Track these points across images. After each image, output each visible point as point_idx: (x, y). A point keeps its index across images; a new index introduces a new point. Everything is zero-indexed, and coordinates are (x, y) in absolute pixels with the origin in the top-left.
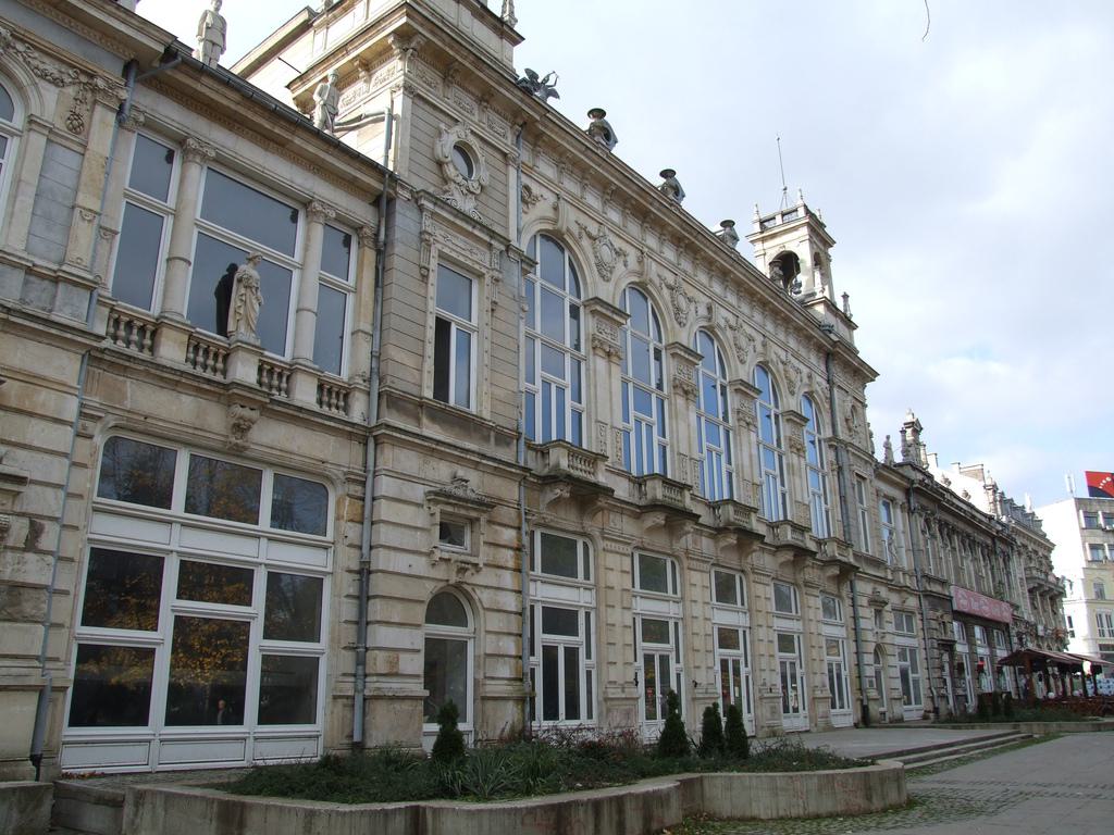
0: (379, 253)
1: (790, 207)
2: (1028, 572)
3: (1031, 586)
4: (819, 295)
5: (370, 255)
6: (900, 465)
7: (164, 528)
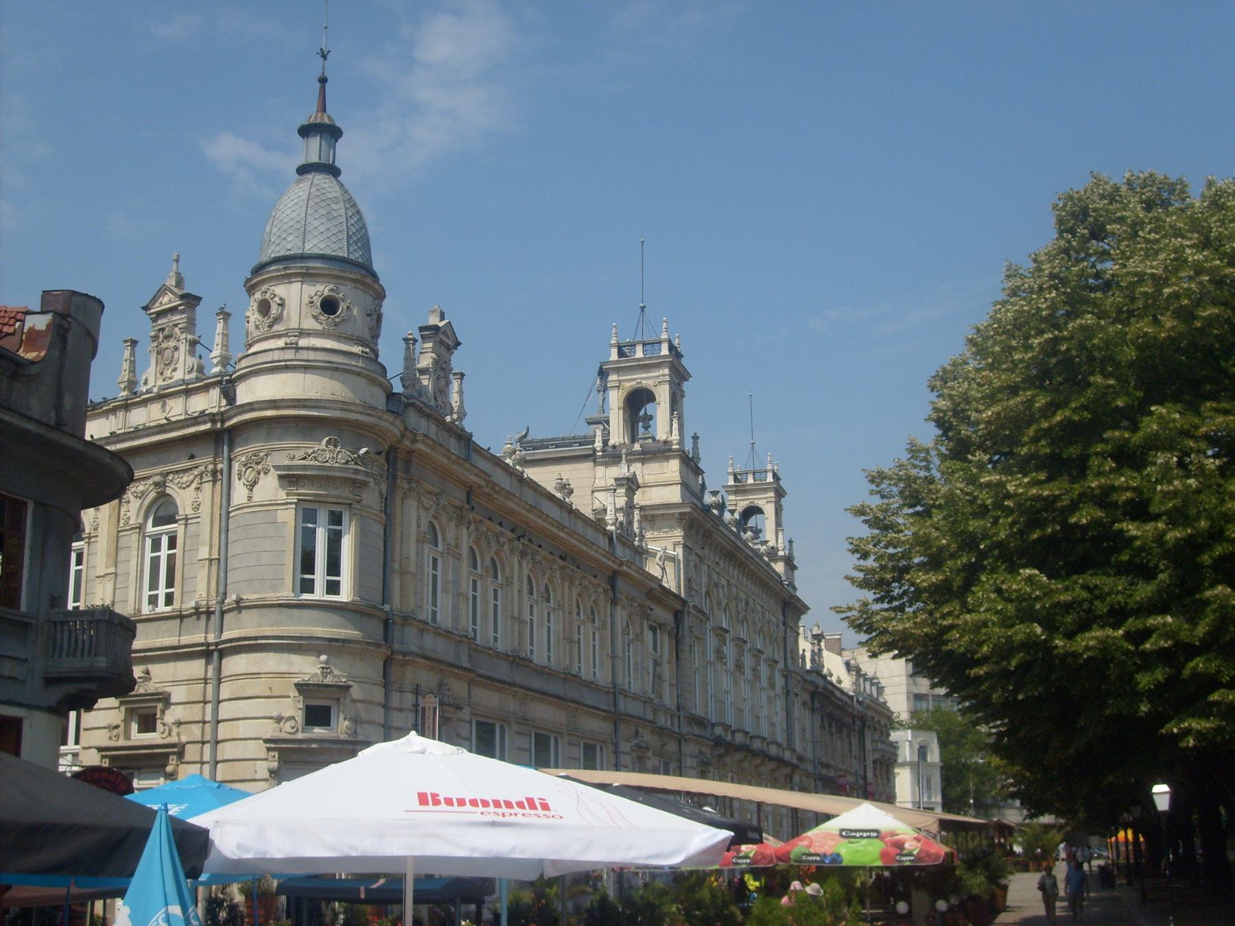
0: (677, 641)
1: (654, 338)
2: (874, 744)
3: (876, 757)
4: (781, 553)
5: (674, 641)
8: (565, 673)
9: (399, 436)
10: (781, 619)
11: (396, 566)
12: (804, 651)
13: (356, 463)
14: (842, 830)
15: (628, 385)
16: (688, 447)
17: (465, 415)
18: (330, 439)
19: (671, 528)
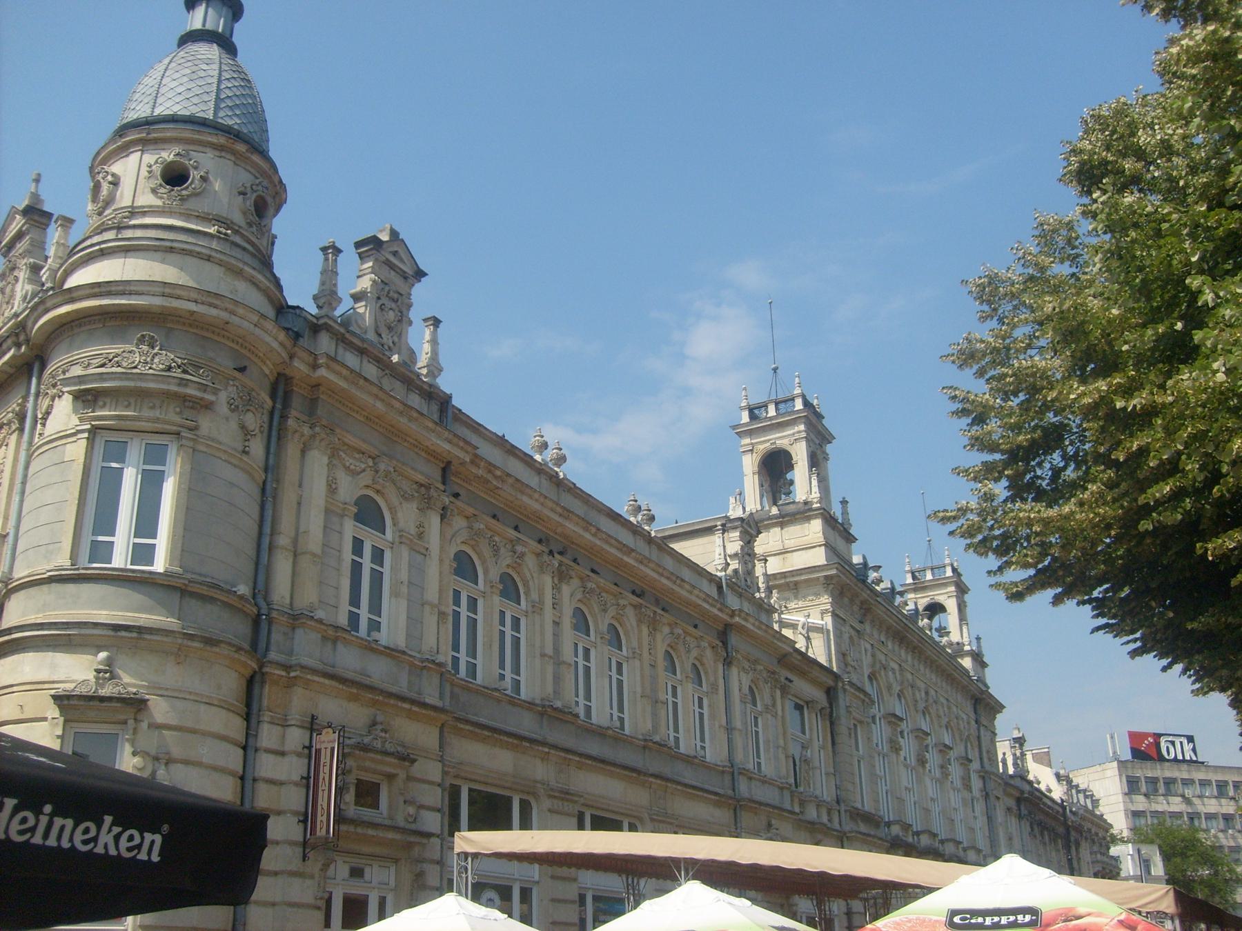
0: (832, 723)
1: (788, 395)
3: (1097, 869)
4: (967, 648)
5: (828, 723)
6: (1011, 776)
8: (645, 740)
9: (284, 355)
10: (972, 715)
11: (283, 540)
12: (1004, 754)
13: (185, 372)
14: (954, 913)
15: (761, 447)
16: (836, 510)
17: (441, 370)
18: (143, 336)
19: (817, 595)
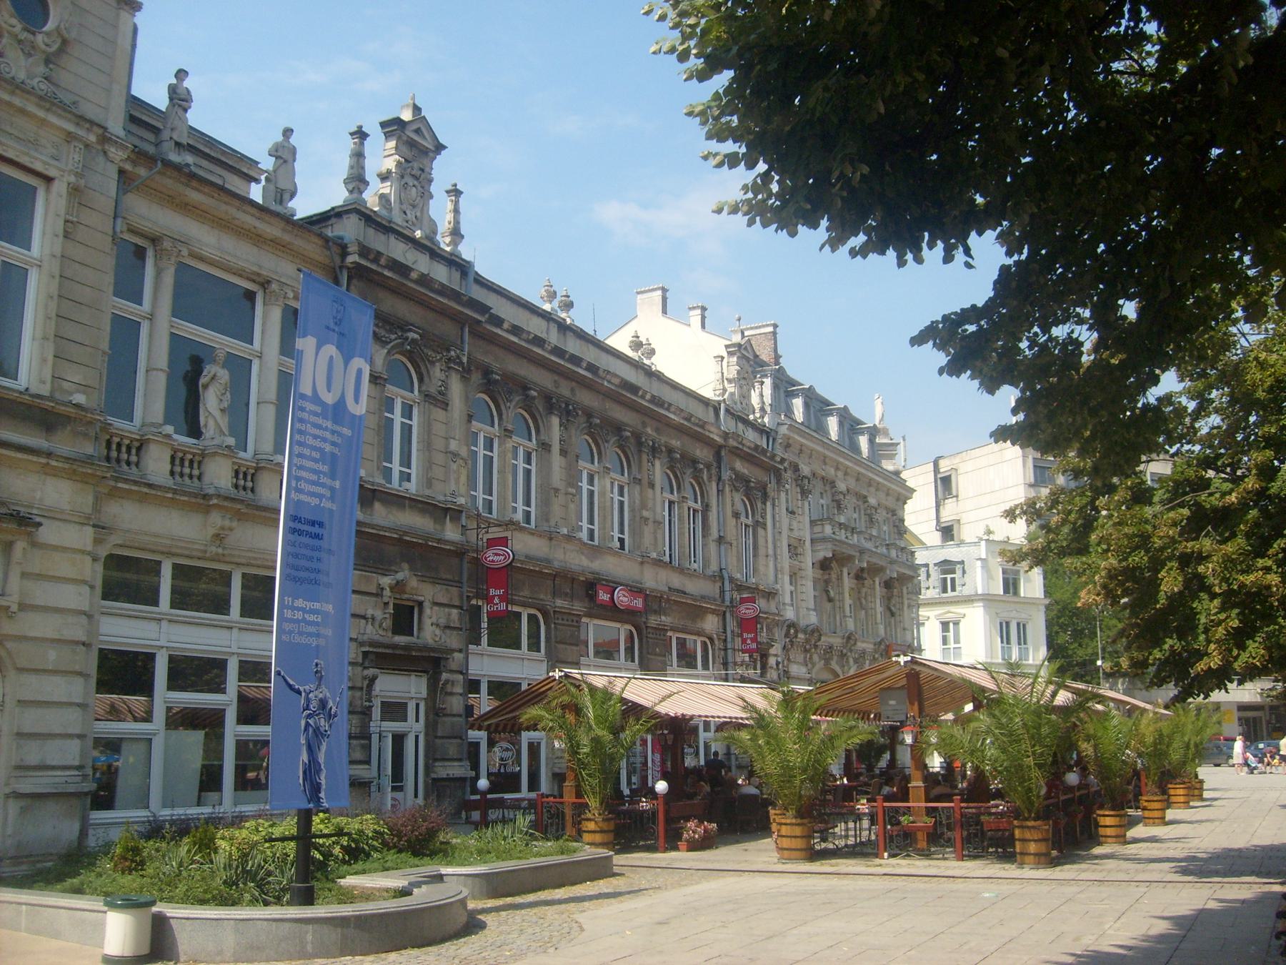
3: (821, 555)
7: (153, 625)
